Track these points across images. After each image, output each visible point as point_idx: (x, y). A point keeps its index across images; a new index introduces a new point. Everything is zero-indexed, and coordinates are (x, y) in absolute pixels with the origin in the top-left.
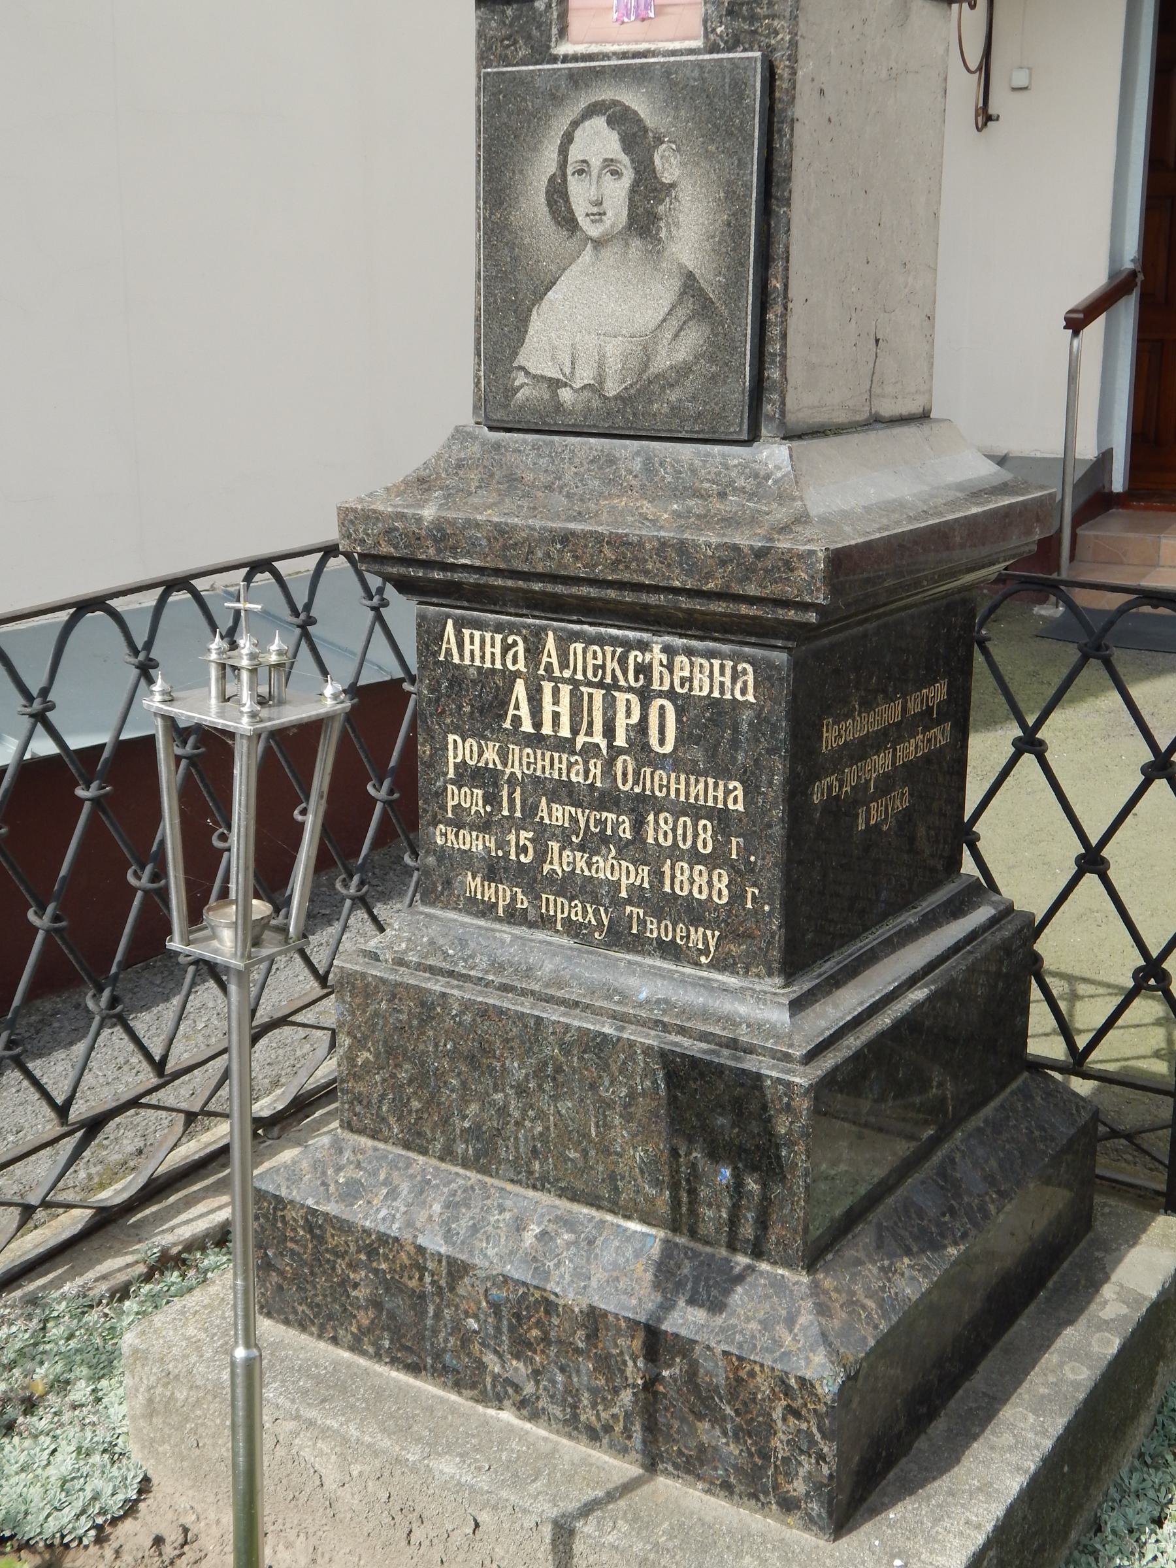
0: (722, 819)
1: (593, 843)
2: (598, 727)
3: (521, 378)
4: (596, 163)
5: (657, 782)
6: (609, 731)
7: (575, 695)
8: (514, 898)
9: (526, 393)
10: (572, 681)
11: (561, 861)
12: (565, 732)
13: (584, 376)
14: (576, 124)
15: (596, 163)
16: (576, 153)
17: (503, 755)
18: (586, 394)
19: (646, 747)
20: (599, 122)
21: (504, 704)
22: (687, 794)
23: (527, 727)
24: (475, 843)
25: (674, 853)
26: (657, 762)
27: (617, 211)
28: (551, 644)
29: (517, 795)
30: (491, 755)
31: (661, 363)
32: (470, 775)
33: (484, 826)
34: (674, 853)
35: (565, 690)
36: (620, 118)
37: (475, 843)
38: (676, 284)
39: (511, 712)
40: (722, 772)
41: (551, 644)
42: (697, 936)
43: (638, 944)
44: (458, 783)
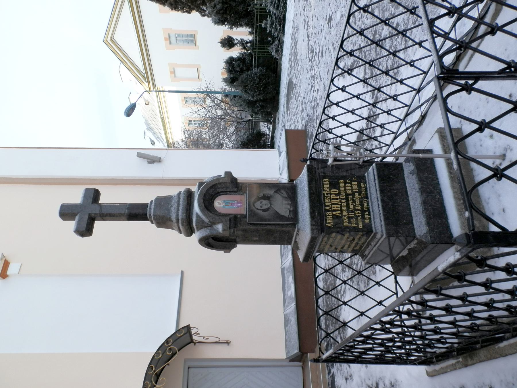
0: (345, 183)
1: (354, 201)
3: (290, 216)
4: (261, 205)
5: (343, 192)
6: (337, 199)
7: (333, 204)
9: (291, 216)
10: (331, 204)
11: (359, 207)
12: (339, 206)
13: (289, 207)
16: (259, 208)
17: (345, 216)
19: (338, 193)
20: (255, 204)
23: (340, 212)
25: (352, 189)
31: (286, 196)
32: (350, 222)
33: (357, 219)
34: (352, 189)
35: (333, 206)
38: (276, 194)
40: (339, 183)
42: (363, 186)
43: (367, 194)
44: (351, 224)
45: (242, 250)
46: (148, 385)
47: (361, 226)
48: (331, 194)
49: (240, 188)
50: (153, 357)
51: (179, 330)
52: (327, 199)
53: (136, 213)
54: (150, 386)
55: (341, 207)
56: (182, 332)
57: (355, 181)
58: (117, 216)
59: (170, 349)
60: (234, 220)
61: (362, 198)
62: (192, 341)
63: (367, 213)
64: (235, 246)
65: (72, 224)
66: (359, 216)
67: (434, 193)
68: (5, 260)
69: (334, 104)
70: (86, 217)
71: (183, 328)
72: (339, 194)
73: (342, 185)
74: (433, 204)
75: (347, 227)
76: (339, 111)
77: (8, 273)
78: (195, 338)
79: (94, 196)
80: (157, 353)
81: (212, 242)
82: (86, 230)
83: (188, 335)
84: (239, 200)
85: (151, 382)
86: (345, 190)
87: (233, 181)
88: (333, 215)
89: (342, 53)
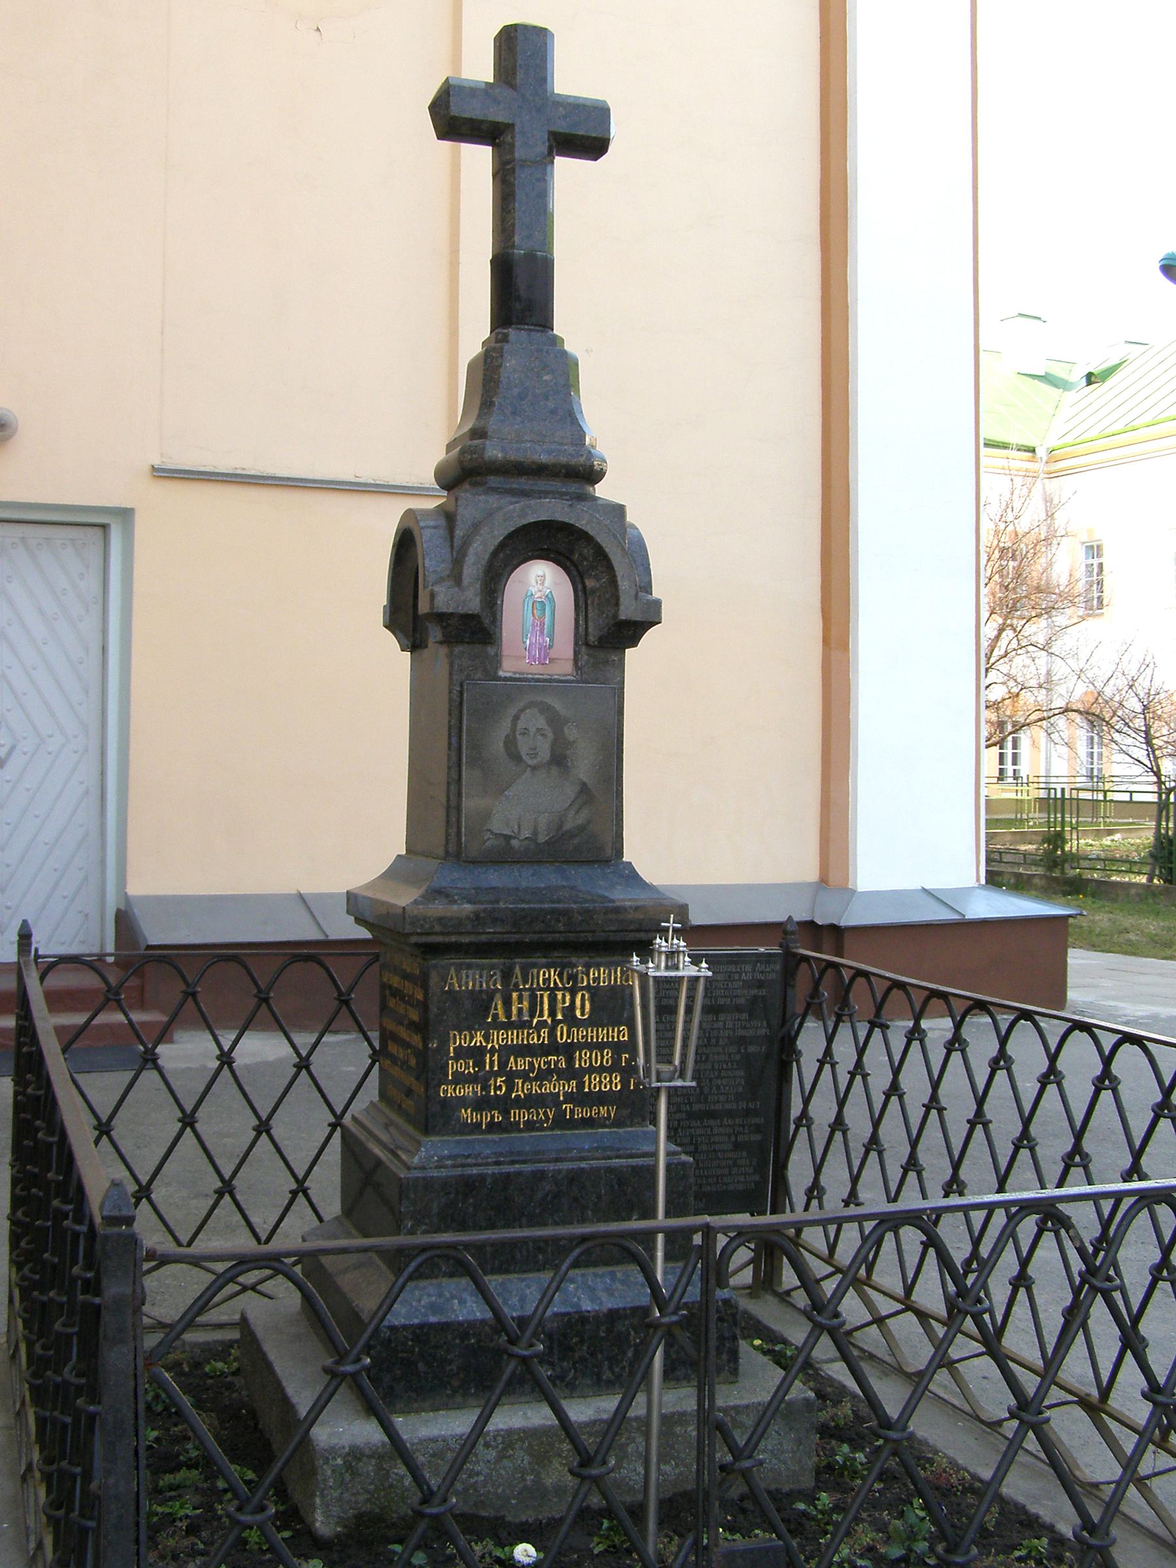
1: (544, 1075)
2: (546, 1013)
4: (533, 730)
5: (579, 1035)
8: (493, 1117)
11: (521, 1089)
14: (522, 710)
15: (533, 730)
16: (521, 725)
17: (487, 1038)
18: (527, 842)
21: (488, 1009)
22: (598, 1038)
24: (467, 1091)
25: (591, 1070)
27: (545, 754)
28: (517, 970)
29: (496, 1058)
30: (479, 1039)
31: (568, 826)
32: (461, 1053)
33: (472, 1079)
34: (591, 1070)
35: (526, 994)
37: (467, 1091)
39: (492, 1011)
41: (517, 970)
44: (456, 1058)
47: (448, 1091)
49: (601, 655)
53: (521, 290)
55: (522, 1025)
60: (475, 631)
61: (558, 1104)
63: (498, 1118)
66: (485, 1088)
67: (561, 1360)
70: (499, 115)
72: (570, 1019)
73: (602, 1034)
75: (444, 1043)
79: (586, 137)
82: (454, 117)
84: (553, 653)
86: (591, 1046)
87: (629, 632)
88: (491, 996)
89: (1107, 1041)
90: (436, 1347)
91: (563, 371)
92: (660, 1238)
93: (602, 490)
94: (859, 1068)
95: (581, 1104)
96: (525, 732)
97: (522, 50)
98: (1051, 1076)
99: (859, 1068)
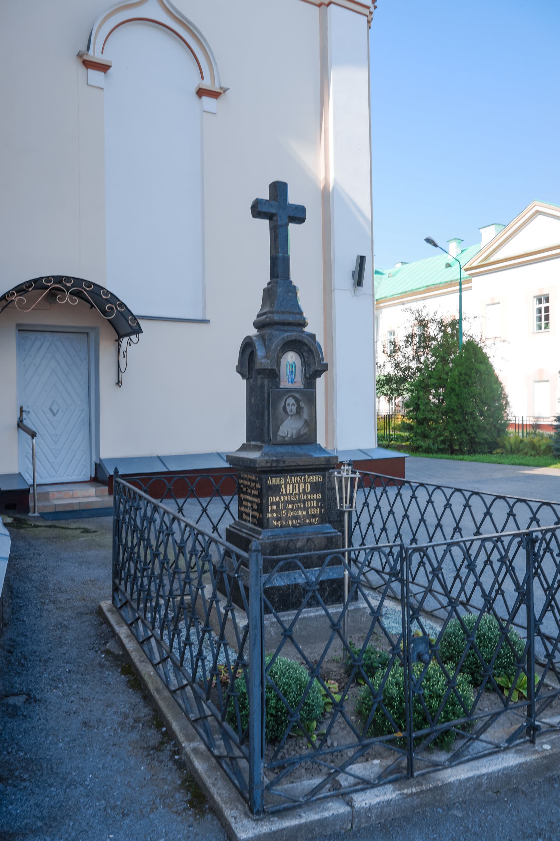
0: (318, 501)
1: (297, 510)
5: (307, 497)
6: (299, 490)
7: (293, 486)
12: (291, 492)
13: (289, 435)
16: (287, 402)
17: (280, 498)
20: (291, 398)
21: (280, 490)
23: (284, 493)
25: (310, 507)
26: (307, 493)
30: (278, 499)
31: (302, 433)
34: (310, 507)
35: (291, 485)
36: (294, 397)
37: (274, 515)
38: (304, 421)
44: (271, 505)
45: (239, 386)
46: (69, 282)
48: (305, 483)
50: (103, 288)
51: (136, 319)
52: (299, 479)
53: (279, 264)
54: (68, 285)
56: (133, 323)
57: (320, 511)
58: (275, 244)
59: (112, 309)
60: (273, 375)
62: (120, 336)
64: (243, 376)
65: (265, 195)
68: (220, 93)
69: (414, 492)
70: (273, 211)
71: (138, 324)
74: (294, 595)
76: (406, 500)
77: (204, 98)
78: (125, 340)
79: (298, 215)
80: (108, 293)
81: (247, 347)
82: (258, 210)
83: (130, 331)
85: (73, 286)
86: (310, 500)
90: (271, 594)
91: (292, 290)
92: (347, 553)
93: (307, 329)
94: (378, 507)
95: (308, 518)
96: (289, 405)
97: (278, 189)
98: (448, 505)
99: (378, 507)
